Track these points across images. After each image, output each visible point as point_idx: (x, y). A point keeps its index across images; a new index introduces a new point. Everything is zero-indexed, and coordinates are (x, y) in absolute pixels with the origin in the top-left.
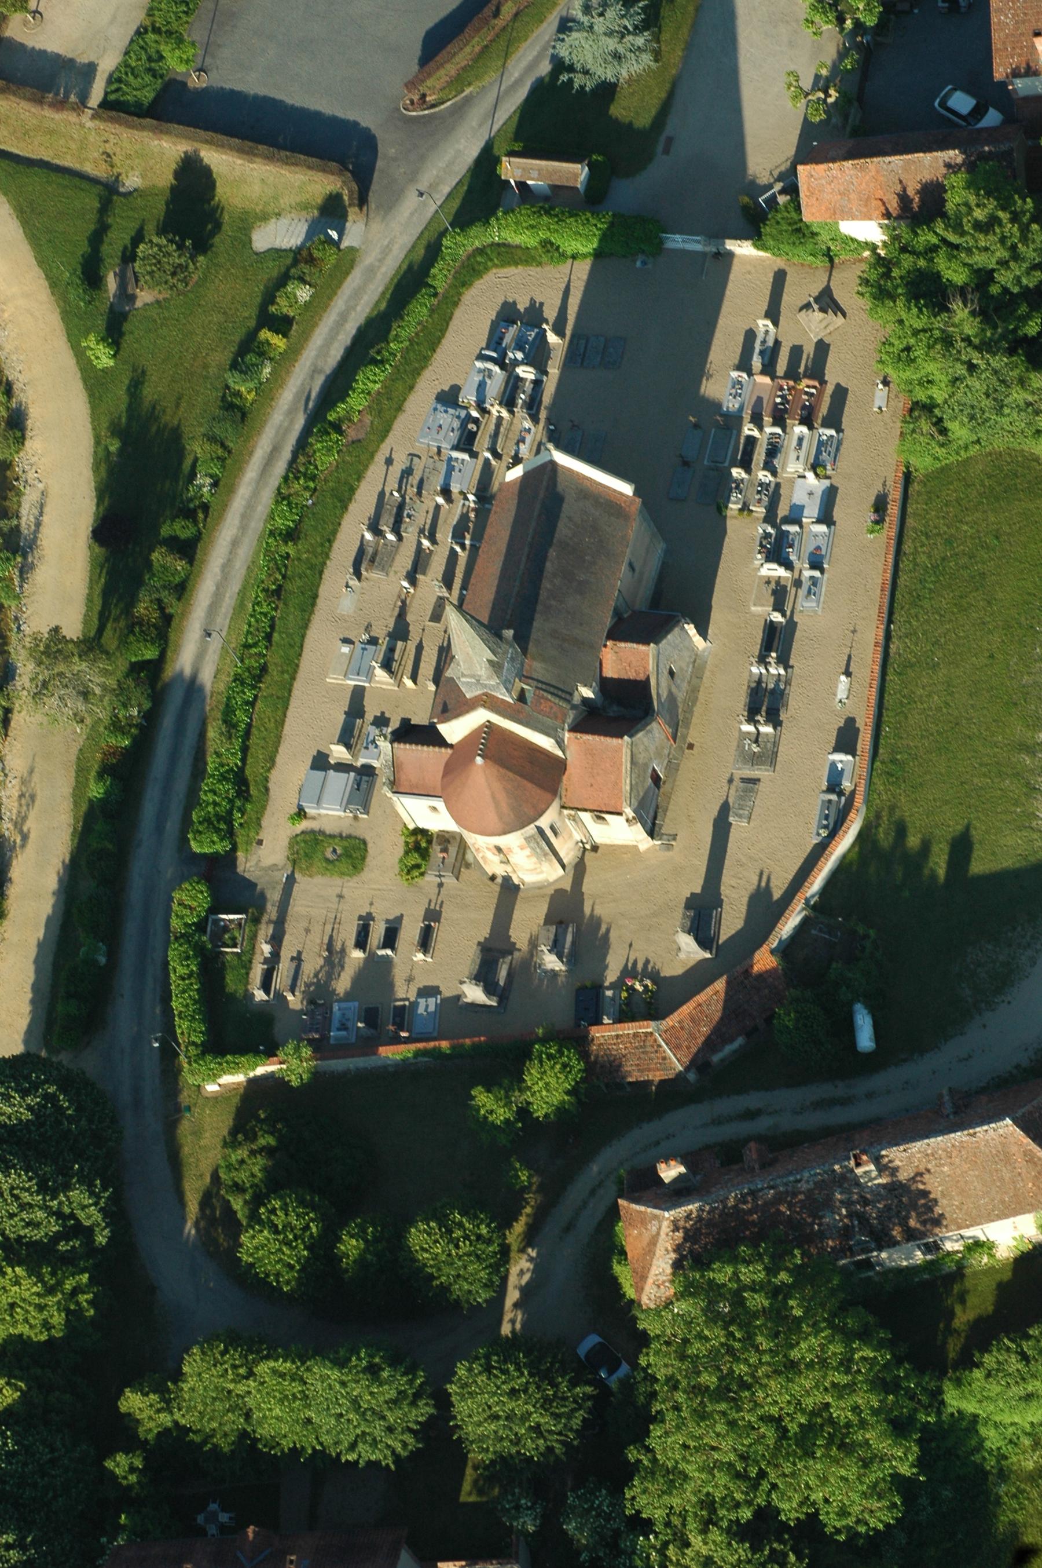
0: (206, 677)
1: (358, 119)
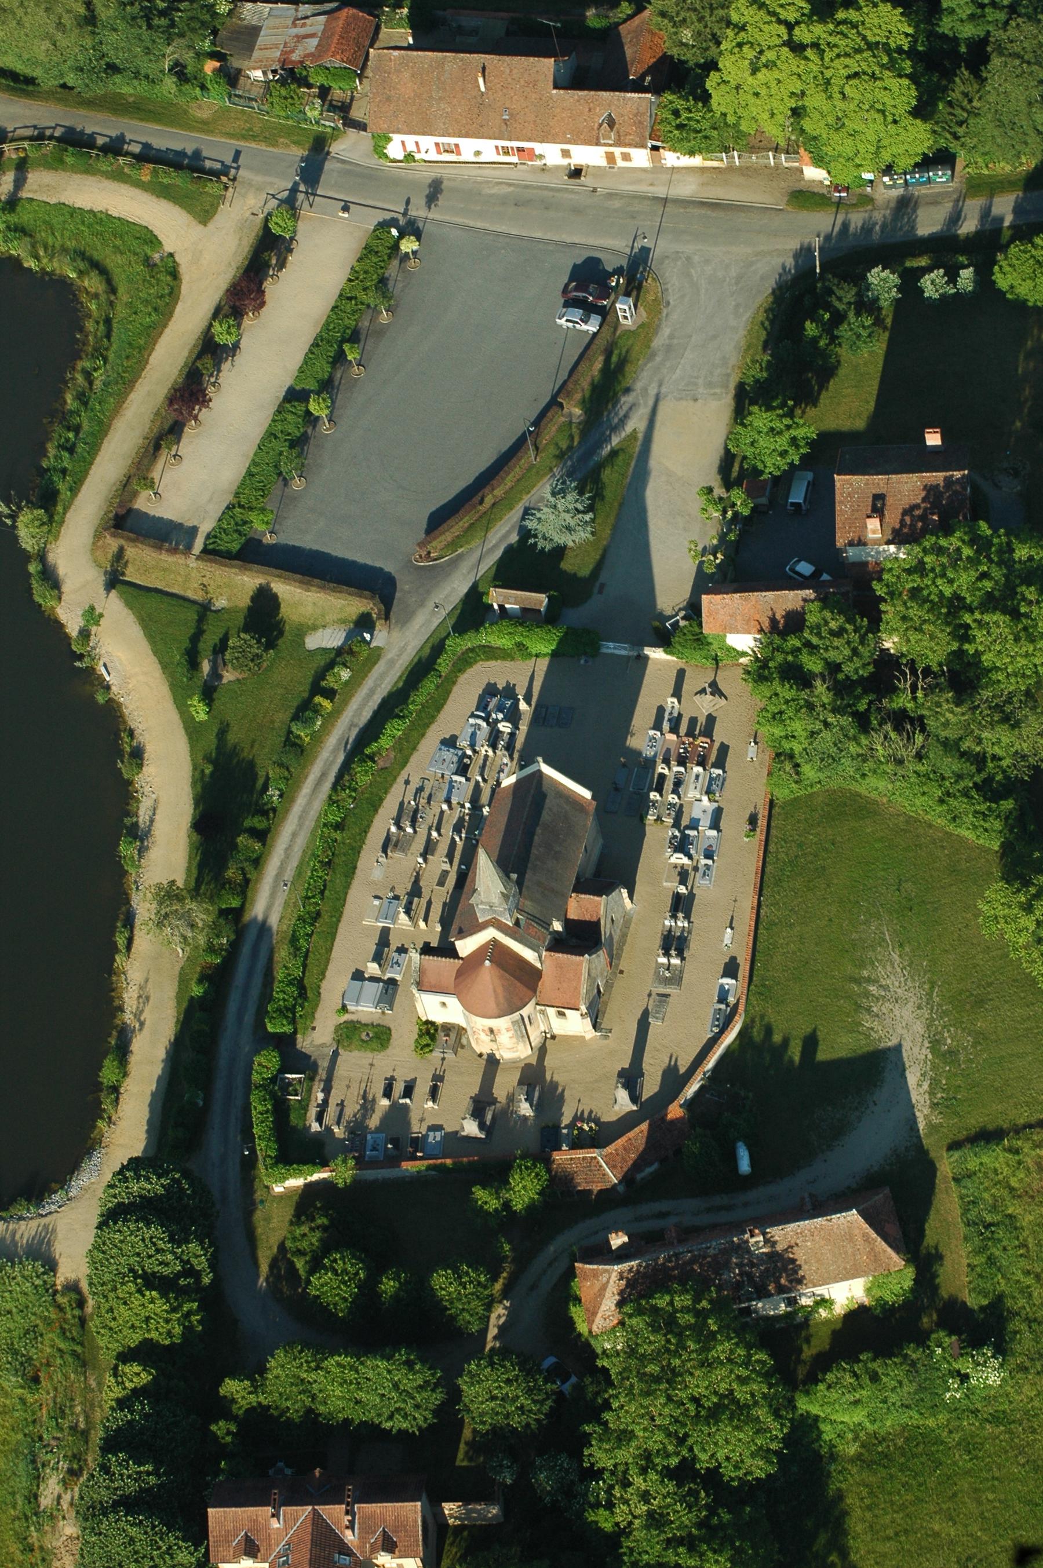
0: (274, 921)
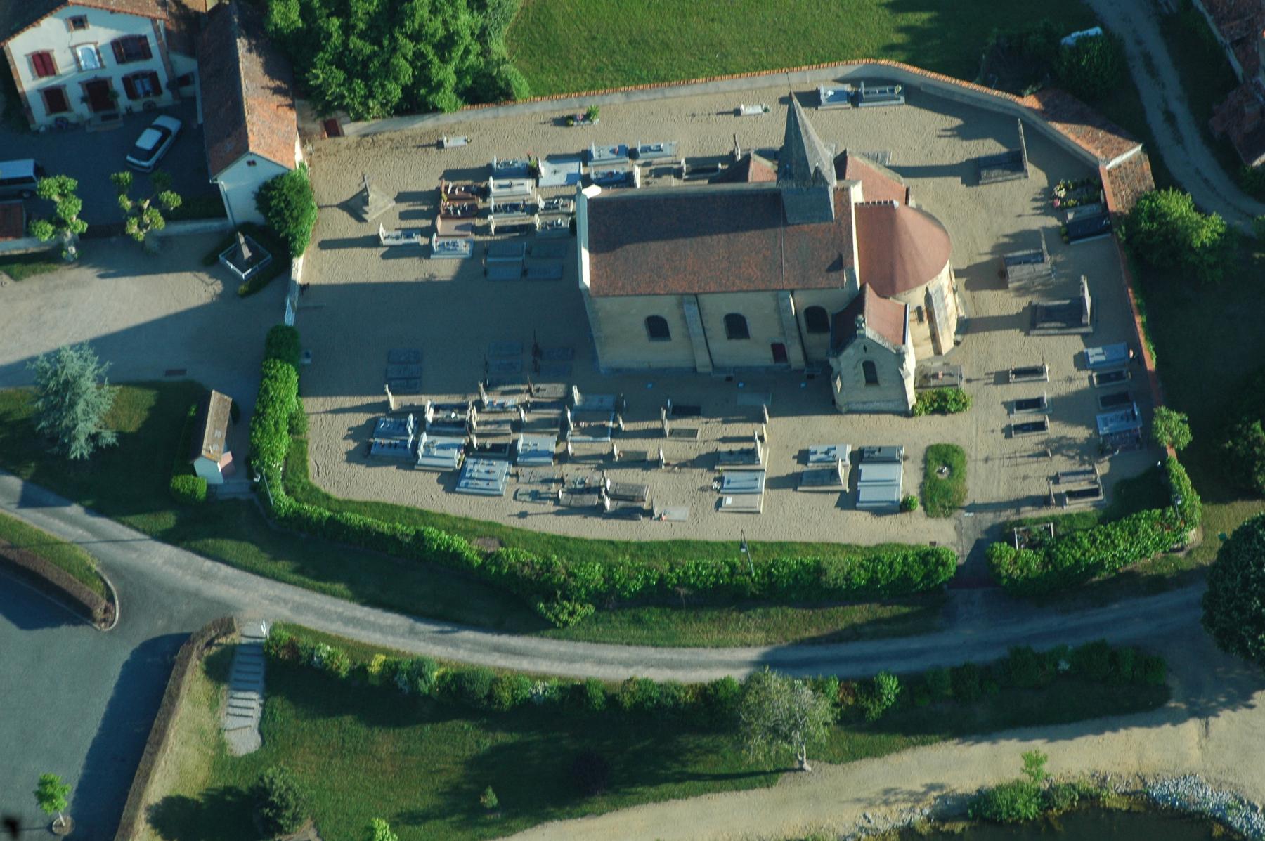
0: (752, 654)
1: (121, 663)
